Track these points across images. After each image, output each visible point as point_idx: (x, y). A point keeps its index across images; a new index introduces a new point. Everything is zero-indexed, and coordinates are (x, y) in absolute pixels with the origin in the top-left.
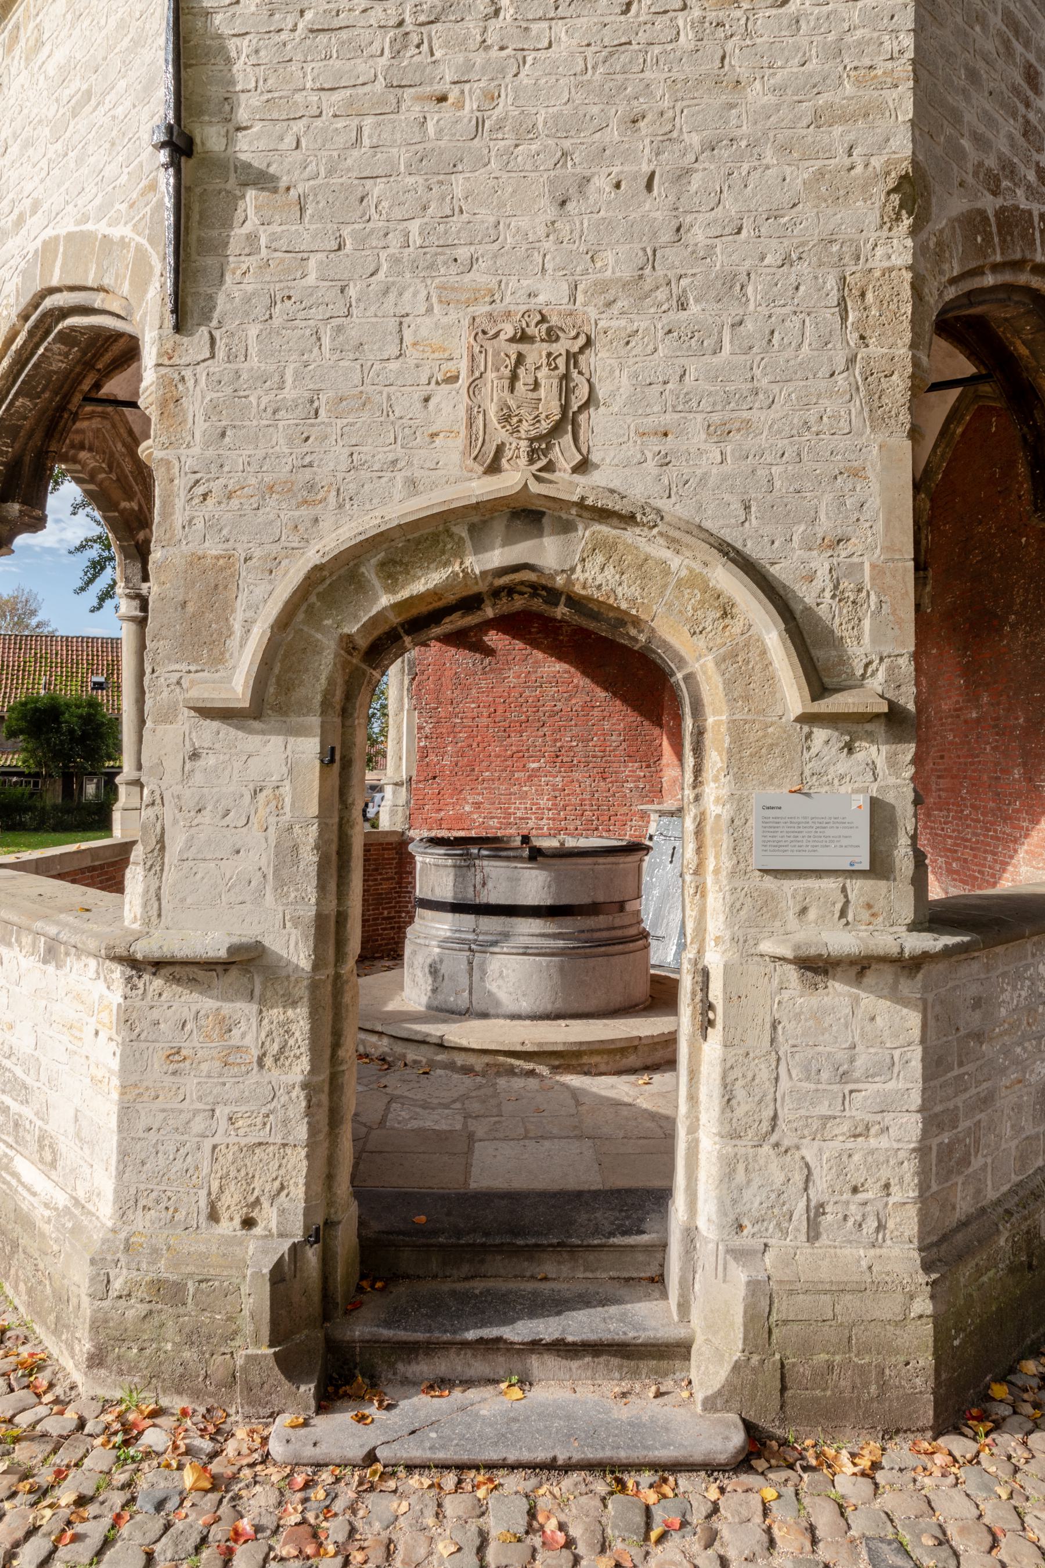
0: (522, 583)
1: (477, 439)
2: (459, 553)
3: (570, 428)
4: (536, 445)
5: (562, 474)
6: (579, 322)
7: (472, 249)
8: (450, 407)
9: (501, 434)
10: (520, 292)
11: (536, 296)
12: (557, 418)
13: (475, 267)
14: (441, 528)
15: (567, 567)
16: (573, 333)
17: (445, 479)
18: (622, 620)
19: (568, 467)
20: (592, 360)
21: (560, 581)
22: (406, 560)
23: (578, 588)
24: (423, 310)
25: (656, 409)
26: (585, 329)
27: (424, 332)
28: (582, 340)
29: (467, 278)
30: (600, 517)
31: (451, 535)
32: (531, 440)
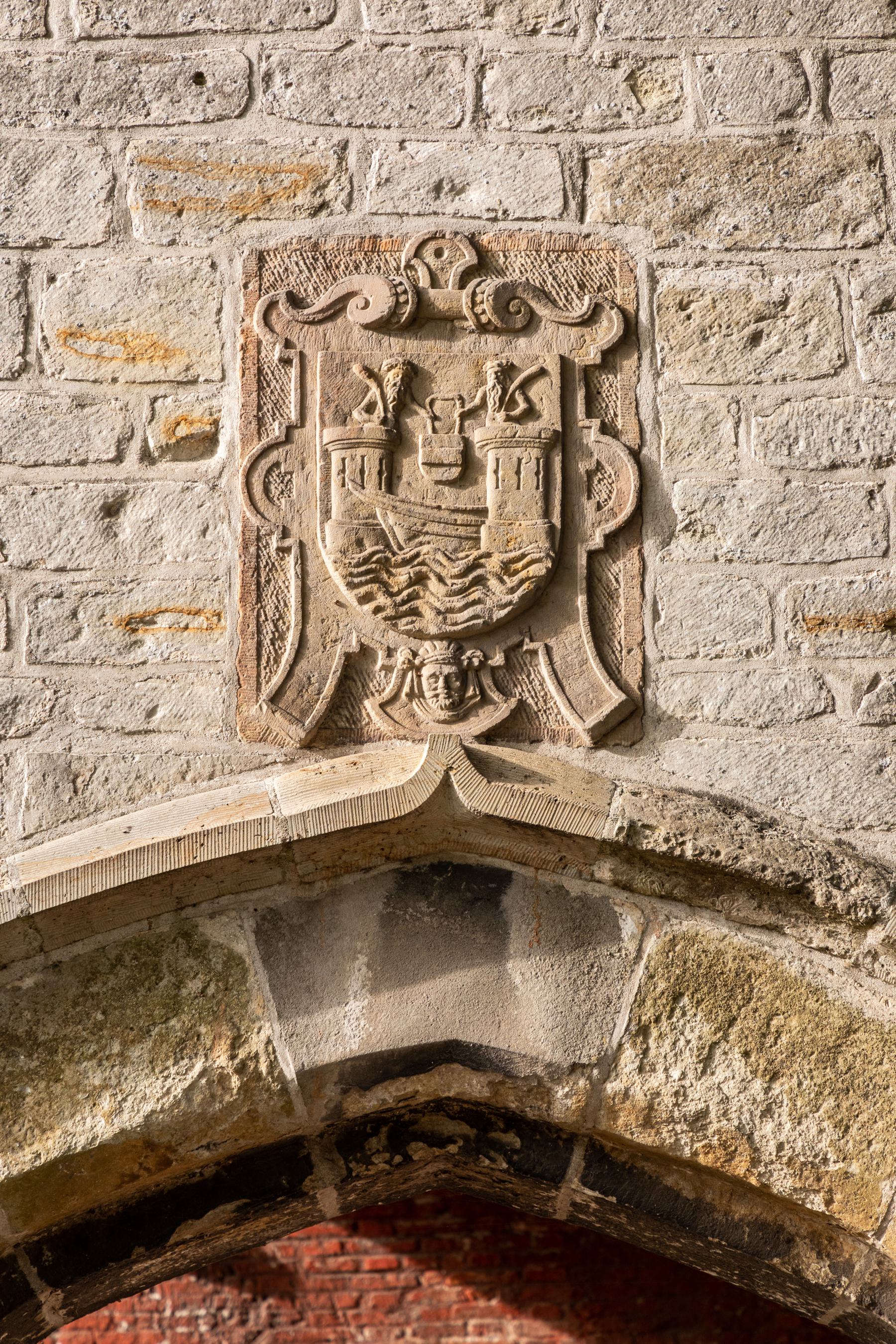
0: (439, 1105)
1: (279, 636)
2: (226, 1009)
3: (581, 601)
4: (472, 655)
5: (561, 750)
6: (598, 271)
7: (252, 46)
8: (188, 533)
9: (359, 622)
10: (407, 181)
11: (457, 191)
12: (539, 570)
13: (261, 100)
14: (165, 925)
15: (588, 1054)
16: (581, 308)
17: (174, 767)
18: (782, 1226)
19: (580, 728)
20: (645, 390)
21: (565, 1101)
22: (48, 1031)
23: (626, 1125)
24: (96, 229)
25: (854, 545)
26: (619, 293)
27: (100, 297)
28: (608, 329)
29: (237, 133)
30: (693, 887)
31: (200, 950)
32: (458, 641)
